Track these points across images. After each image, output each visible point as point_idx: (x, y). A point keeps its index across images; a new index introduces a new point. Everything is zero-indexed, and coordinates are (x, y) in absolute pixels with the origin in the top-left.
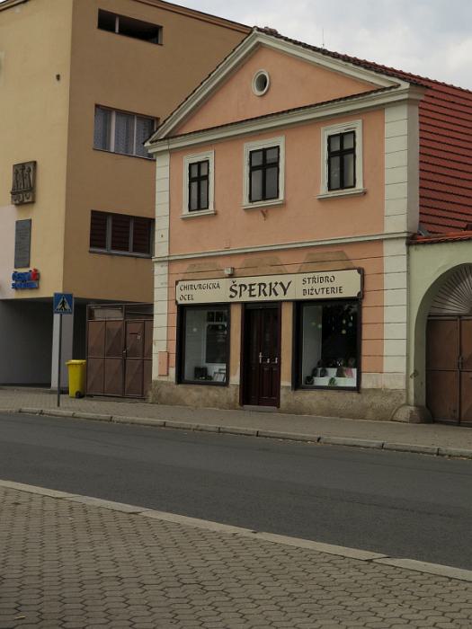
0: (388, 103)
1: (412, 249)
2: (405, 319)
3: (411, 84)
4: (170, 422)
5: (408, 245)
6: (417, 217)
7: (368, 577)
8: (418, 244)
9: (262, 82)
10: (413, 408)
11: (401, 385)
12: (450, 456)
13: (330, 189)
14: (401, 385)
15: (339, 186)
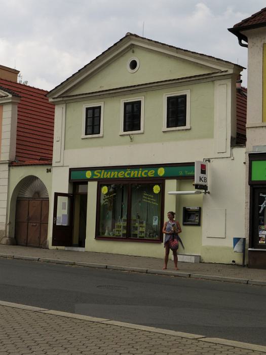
0: (4, 103)
1: (11, 168)
2: (6, 199)
3: (13, 95)
4: (42, 258)
5: (9, 166)
6: (15, 154)
7: (97, 331)
8: (13, 166)
9: (134, 65)
10: (8, 238)
11: (3, 228)
12: (224, 281)
13: (86, 134)
14: (3, 228)
15: (91, 133)
